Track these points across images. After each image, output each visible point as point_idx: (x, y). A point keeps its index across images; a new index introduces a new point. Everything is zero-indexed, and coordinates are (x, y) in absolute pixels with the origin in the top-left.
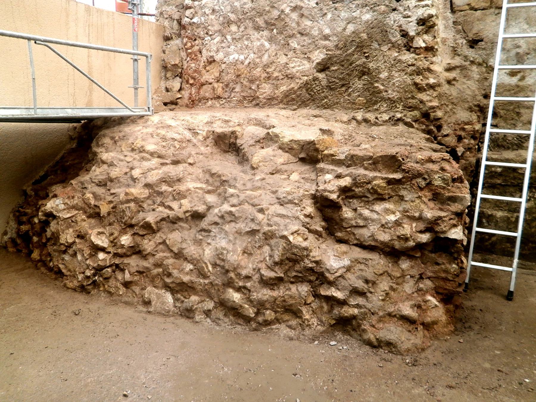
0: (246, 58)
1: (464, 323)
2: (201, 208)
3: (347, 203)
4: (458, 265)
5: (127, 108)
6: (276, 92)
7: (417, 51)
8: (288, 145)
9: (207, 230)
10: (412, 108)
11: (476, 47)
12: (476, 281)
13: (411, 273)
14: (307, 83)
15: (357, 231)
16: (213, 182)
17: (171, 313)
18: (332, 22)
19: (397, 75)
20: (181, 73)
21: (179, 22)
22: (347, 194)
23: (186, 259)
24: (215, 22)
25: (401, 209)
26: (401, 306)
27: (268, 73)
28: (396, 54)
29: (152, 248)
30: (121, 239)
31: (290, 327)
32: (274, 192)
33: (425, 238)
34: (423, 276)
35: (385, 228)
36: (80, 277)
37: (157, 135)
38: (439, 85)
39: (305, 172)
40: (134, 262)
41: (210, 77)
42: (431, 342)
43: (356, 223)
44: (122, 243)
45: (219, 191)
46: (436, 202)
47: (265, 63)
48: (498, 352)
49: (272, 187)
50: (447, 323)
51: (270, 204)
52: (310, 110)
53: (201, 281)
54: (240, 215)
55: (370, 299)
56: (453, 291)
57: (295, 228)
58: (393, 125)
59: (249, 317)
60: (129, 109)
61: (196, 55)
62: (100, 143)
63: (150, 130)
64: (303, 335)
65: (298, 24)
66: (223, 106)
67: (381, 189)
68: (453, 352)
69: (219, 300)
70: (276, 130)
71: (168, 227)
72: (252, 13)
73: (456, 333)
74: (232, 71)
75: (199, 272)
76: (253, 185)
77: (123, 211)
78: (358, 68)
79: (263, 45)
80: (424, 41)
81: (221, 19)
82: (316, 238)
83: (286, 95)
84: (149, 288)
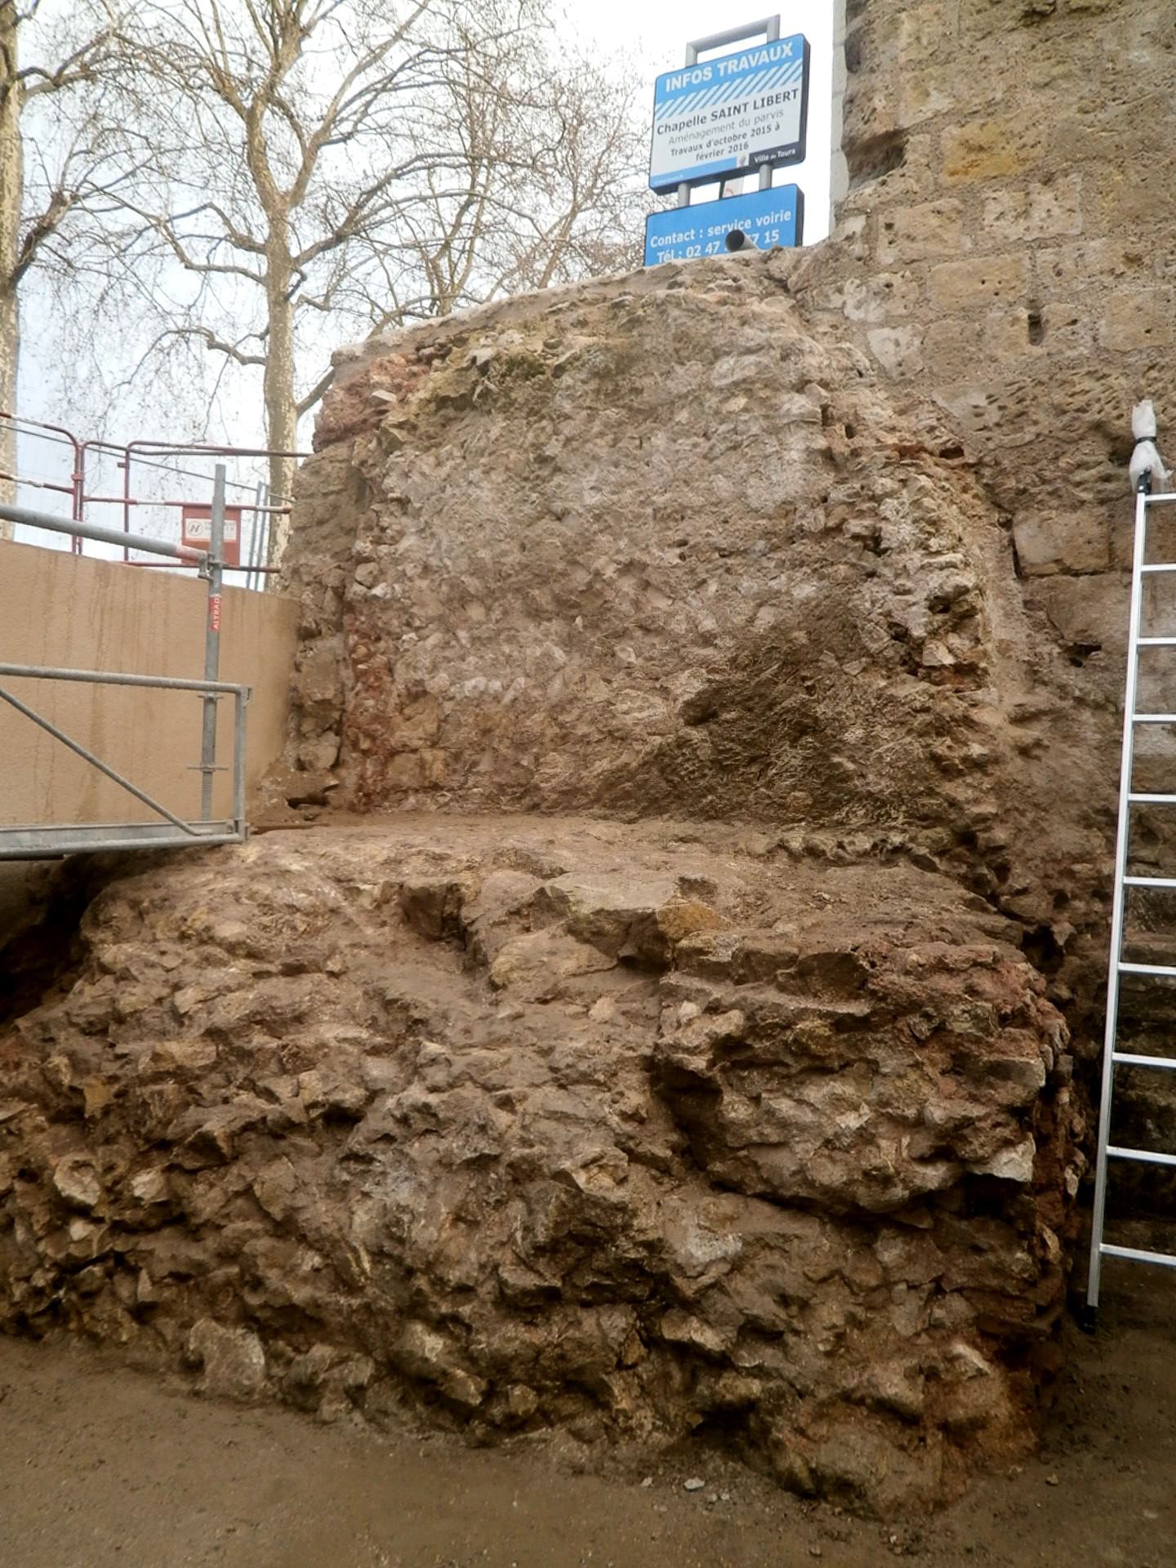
0: (506, 688)
1: (1070, 1427)
2: (351, 1096)
3: (735, 1081)
4: (1030, 1251)
5: (176, 824)
6: (584, 773)
7: (934, 674)
8: (591, 923)
9: (363, 1157)
10: (929, 820)
11: (1085, 663)
12: (1126, 1301)
13: (911, 1277)
14: (661, 753)
15: (766, 1158)
16: (387, 1023)
17: (256, 1397)
18: (719, 601)
19: (886, 734)
20: (340, 722)
21: (339, 593)
22: (735, 1058)
23: (303, 1239)
24: (429, 597)
25: (873, 1096)
26: (878, 1370)
27: (562, 726)
28: (883, 683)
29: (216, 1206)
30: (134, 1183)
31: (577, 1435)
32: (546, 1052)
33: (933, 1176)
34: (944, 1285)
35: (834, 1149)
36: (18, 1291)
37: (251, 897)
38: (996, 760)
39: (631, 997)
40: (165, 1249)
41: (415, 734)
42: (969, 1482)
43: (761, 1134)
44: (137, 1193)
45: (402, 1048)
46: (961, 1079)
47: (554, 701)
48: (1151, 1515)
49: (540, 1038)
50: (1017, 1426)
51: (533, 1085)
52: (672, 823)
53: (342, 1300)
54: (451, 1114)
55: (794, 1352)
56: (1023, 1328)
57: (594, 1150)
58: (883, 864)
59: (466, 1405)
60: (182, 827)
61: (378, 679)
62: (101, 918)
63: (231, 883)
64: (613, 1459)
65: (636, 604)
66: (445, 809)
67: (817, 1044)
68: (1024, 1514)
69: (387, 1356)
70: (562, 884)
71: (262, 1149)
72: (521, 577)
73: (1044, 1455)
74: (471, 720)
75: (338, 1275)
76: (489, 1034)
77: (145, 1104)
78: (788, 717)
79: (548, 656)
80: (950, 651)
81: (445, 588)
82: (654, 1178)
83: (611, 782)
84: (201, 1324)
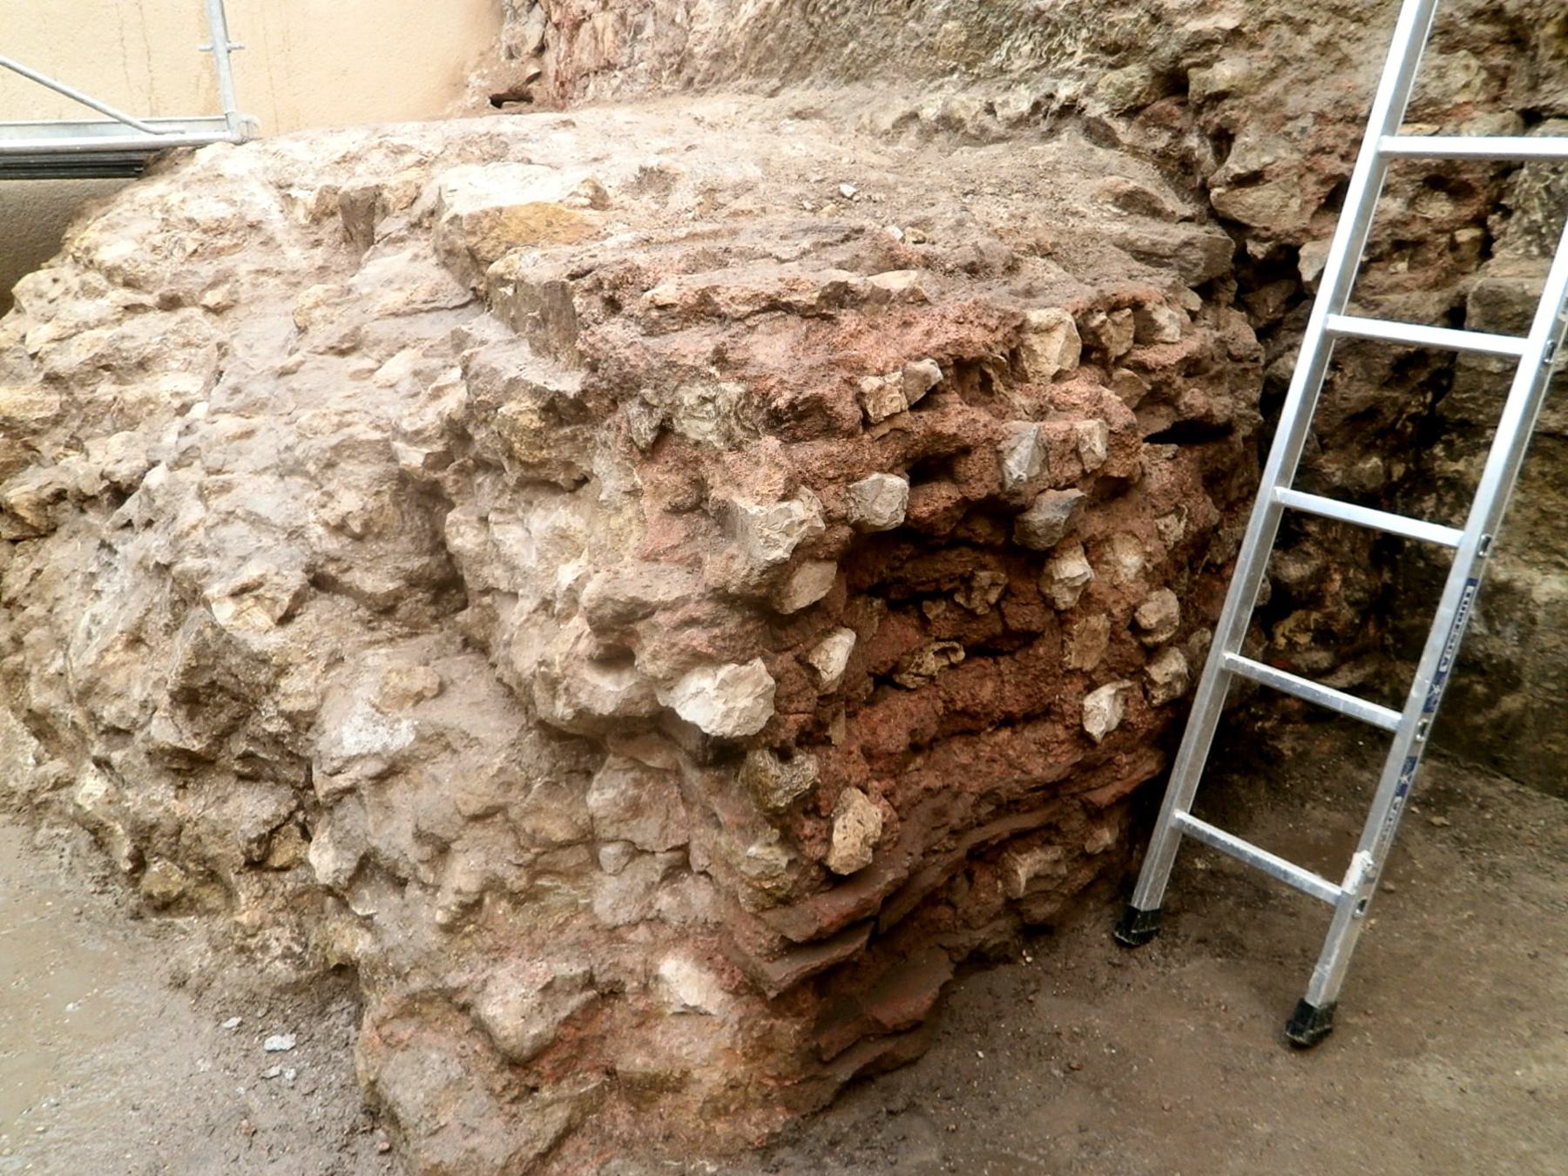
6: (731, 26)
10: (1118, 52)
39: (443, 349)
